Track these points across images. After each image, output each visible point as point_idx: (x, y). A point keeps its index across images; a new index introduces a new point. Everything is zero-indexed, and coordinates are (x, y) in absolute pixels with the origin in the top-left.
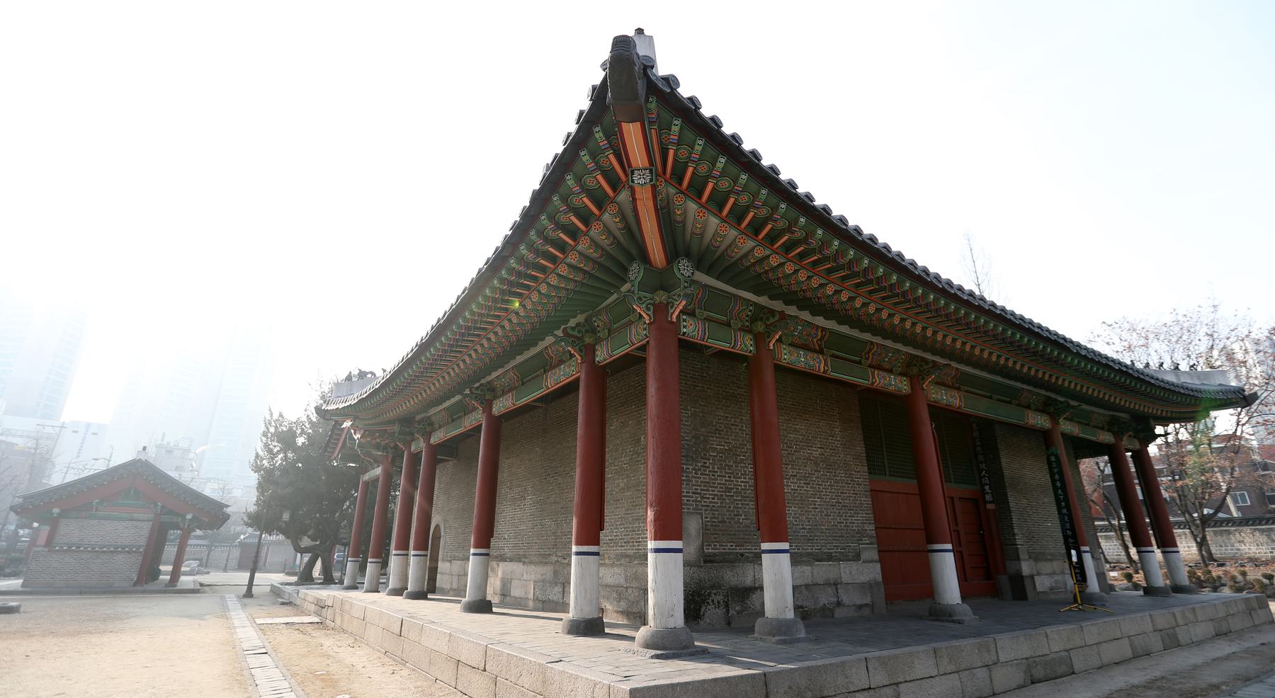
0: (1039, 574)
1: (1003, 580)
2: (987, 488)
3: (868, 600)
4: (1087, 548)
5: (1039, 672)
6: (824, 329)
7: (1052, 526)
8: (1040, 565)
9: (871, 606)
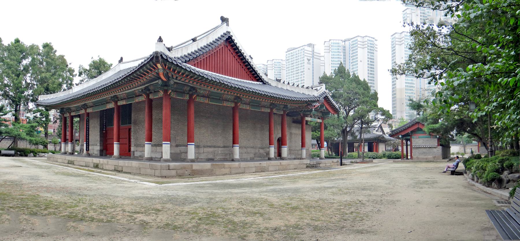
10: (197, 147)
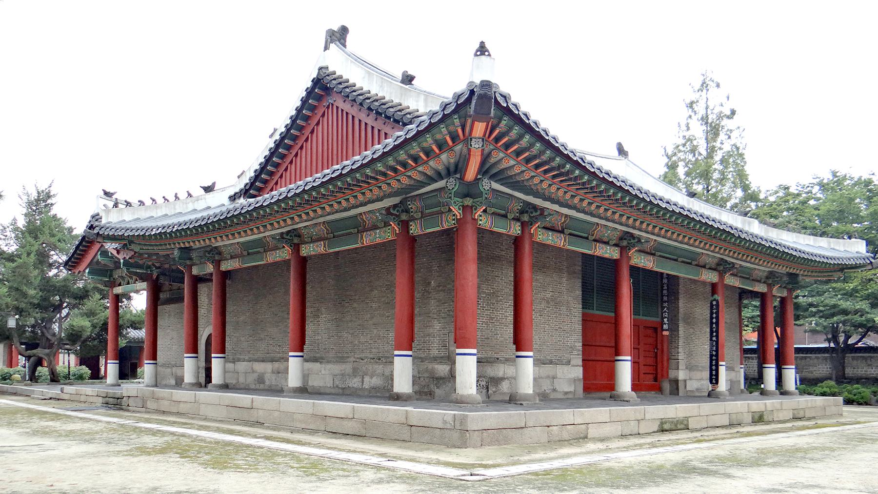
0: (690, 379)
1: (666, 386)
2: (665, 320)
3: (572, 389)
4: (723, 363)
5: (666, 427)
6: (566, 216)
7: (704, 348)
8: (693, 373)
9: (574, 393)
10: (538, 362)
